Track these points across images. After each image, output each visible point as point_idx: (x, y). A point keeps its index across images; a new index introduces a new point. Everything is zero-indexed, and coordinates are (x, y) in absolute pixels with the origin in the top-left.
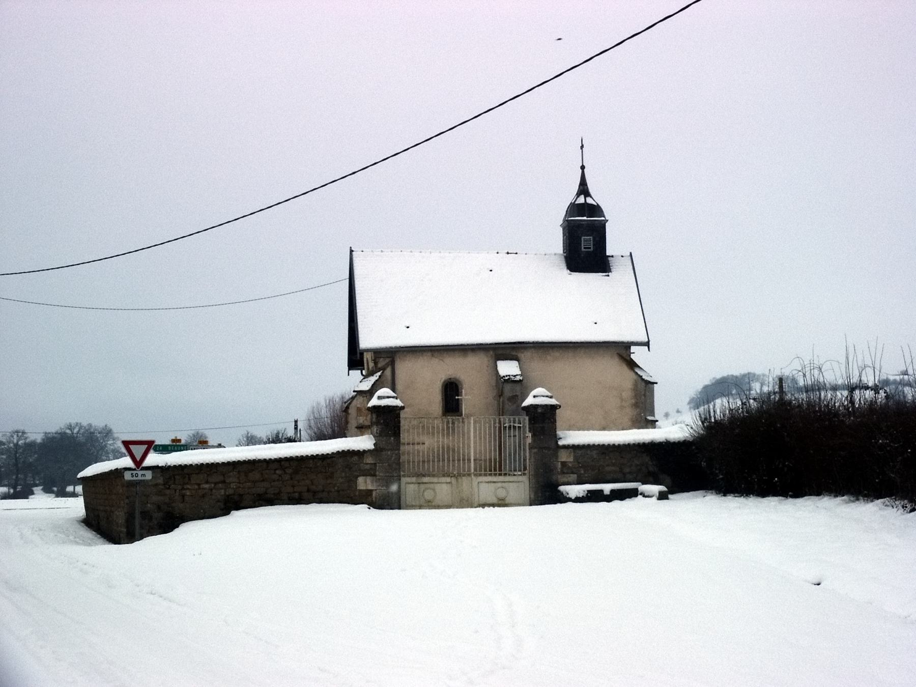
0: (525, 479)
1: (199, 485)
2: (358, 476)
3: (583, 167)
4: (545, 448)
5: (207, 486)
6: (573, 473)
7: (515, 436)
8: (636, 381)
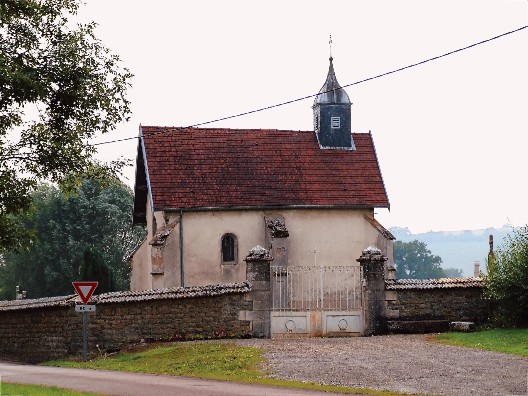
0: (359, 313)
1: (122, 316)
2: (240, 310)
3: (331, 59)
4: (376, 290)
5: (128, 317)
6: (396, 309)
7: (282, 281)
8: (379, 237)
